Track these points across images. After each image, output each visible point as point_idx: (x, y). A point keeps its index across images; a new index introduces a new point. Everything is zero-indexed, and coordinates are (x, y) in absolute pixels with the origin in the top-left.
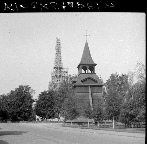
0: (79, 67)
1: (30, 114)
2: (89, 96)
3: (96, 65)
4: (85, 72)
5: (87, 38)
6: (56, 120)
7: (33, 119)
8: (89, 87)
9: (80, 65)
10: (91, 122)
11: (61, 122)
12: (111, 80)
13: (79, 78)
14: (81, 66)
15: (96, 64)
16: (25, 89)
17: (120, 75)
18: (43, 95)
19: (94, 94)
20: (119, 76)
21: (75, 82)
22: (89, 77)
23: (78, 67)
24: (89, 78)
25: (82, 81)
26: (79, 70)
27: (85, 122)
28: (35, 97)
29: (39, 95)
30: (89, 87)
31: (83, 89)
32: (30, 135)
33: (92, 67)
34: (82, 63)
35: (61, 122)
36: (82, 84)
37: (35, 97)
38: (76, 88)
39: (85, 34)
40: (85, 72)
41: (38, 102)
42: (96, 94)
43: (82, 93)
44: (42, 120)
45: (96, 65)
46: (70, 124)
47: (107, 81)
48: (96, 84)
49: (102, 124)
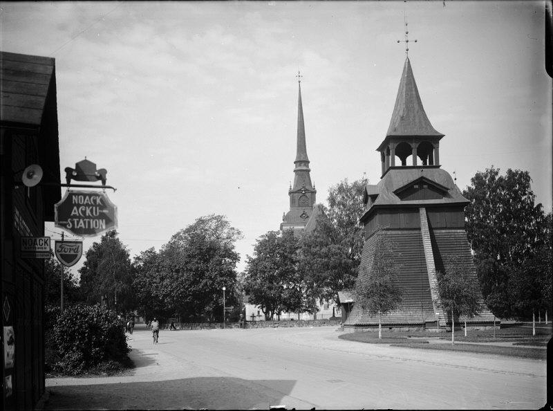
0: (384, 149)
1: (233, 301)
2: (421, 241)
3: (441, 137)
4: (404, 162)
5: (407, 50)
6: (305, 316)
7: (237, 319)
8: (423, 211)
9: (389, 139)
10: (433, 320)
11: (324, 322)
12: (474, 187)
13: (387, 184)
14: (392, 146)
15: (443, 134)
16: (213, 224)
17: (503, 174)
18: (268, 246)
19: (438, 231)
20: (499, 175)
21: (374, 197)
22: (422, 178)
23: (378, 150)
24: (422, 181)
25: (401, 193)
26: (383, 160)
27: (410, 322)
28: (245, 251)
29: (257, 243)
30: (423, 211)
31: (402, 218)
32: (420, 363)
33: (427, 145)
34: (394, 134)
35: (324, 322)
36: (397, 201)
37: (245, 251)
38: (377, 218)
39: (403, 39)
40: (404, 162)
41: (252, 262)
42: (443, 231)
43: (400, 232)
44: (268, 319)
45: (441, 137)
46: (376, 330)
47: (467, 190)
48: (444, 201)
49: (390, 328)
